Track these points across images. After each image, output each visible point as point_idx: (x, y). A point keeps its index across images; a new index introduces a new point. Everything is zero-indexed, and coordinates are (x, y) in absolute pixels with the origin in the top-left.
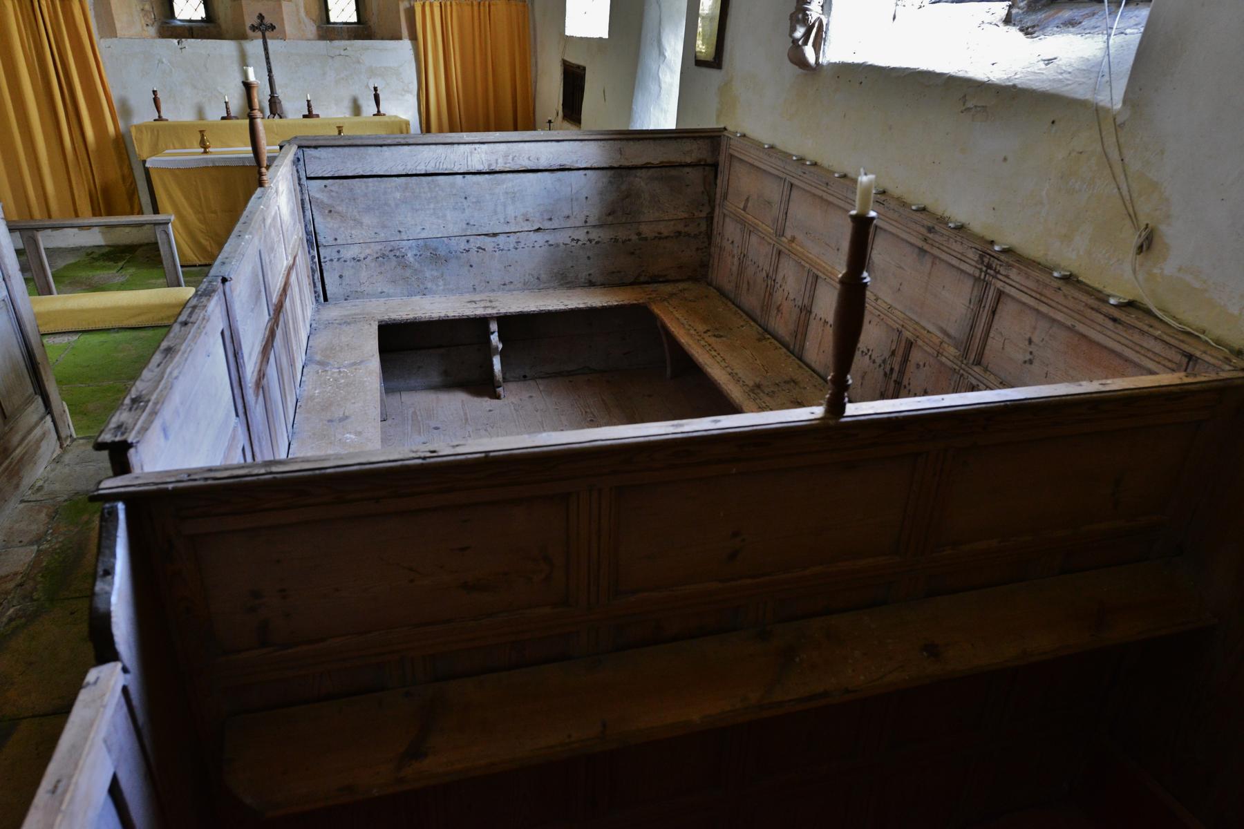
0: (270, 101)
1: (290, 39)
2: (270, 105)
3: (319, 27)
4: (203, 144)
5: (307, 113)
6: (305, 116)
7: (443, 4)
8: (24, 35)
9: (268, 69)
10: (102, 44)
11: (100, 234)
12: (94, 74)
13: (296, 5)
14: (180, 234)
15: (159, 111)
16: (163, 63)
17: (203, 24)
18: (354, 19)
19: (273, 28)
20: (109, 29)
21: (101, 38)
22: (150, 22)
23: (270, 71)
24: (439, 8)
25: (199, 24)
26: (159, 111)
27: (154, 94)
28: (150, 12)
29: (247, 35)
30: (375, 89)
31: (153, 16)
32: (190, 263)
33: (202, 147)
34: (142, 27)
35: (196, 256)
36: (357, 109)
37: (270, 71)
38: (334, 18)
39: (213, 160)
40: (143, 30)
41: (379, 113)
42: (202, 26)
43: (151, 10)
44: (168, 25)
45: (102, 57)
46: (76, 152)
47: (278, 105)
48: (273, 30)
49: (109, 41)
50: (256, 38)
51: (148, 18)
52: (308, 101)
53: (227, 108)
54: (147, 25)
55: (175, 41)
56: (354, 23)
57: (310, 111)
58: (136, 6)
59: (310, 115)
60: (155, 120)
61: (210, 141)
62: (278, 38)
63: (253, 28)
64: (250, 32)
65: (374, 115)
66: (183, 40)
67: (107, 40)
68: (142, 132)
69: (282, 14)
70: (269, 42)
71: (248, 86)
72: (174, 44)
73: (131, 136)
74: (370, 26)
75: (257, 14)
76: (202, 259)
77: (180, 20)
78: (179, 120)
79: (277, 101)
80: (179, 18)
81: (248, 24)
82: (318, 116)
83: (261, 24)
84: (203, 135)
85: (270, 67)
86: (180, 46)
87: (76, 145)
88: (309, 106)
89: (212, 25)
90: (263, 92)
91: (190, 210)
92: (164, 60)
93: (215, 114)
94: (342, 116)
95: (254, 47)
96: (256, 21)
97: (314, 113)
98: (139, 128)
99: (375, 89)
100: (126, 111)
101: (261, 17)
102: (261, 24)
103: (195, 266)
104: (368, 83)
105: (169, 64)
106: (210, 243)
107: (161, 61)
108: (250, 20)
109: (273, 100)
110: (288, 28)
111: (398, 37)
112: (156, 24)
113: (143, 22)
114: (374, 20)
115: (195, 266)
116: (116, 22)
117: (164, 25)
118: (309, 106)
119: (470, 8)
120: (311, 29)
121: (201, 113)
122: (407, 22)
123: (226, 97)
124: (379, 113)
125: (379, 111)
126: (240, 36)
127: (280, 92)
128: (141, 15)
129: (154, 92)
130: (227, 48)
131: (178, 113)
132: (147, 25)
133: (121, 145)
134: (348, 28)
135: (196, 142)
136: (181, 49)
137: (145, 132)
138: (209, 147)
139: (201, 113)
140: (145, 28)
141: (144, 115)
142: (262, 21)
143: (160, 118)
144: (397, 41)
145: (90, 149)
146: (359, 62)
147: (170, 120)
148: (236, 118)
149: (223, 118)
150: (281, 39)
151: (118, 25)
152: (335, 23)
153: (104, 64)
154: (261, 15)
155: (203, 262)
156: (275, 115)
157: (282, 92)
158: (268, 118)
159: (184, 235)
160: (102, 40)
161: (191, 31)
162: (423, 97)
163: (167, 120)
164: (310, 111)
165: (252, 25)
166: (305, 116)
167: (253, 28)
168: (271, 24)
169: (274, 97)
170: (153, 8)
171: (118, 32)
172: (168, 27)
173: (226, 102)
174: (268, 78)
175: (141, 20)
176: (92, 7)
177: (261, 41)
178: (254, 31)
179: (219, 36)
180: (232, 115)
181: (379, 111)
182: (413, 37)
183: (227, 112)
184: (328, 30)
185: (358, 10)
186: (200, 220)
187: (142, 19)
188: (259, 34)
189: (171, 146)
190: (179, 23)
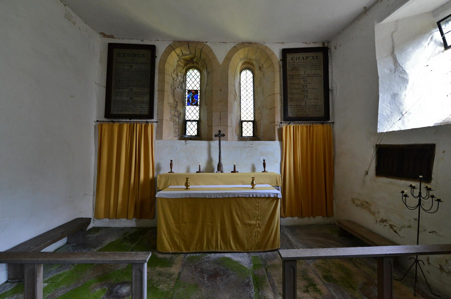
0: (218, 165)
1: (229, 141)
2: (218, 167)
3: (238, 138)
4: (187, 185)
5: (233, 171)
6: (232, 172)
7: (295, 126)
8: (128, 138)
9: (219, 152)
10: (155, 142)
11: (135, 221)
12: (150, 152)
13: (233, 129)
14: (165, 235)
15: (171, 169)
16: (177, 149)
17: (196, 137)
18: (252, 135)
19: (224, 135)
20: (160, 136)
21: (156, 140)
22: (176, 136)
23: (220, 153)
24: (293, 128)
25: (194, 137)
26: (171, 169)
27: (171, 162)
28: (177, 132)
29: (212, 139)
30: (264, 160)
31: (178, 134)
32: (167, 252)
33: (186, 186)
34: (173, 137)
35: (171, 248)
36: (254, 169)
37: (220, 153)
38: (244, 135)
39: (190, 194)
40: (173, 138)
41: (265, 171)
42: (195, 138)
43: (178, 131)
44: (182, 137)
45: (154, 147)
46: (135, 187)
47: (221, 167)
48: (224, 136)
49: (159, 141)
50: (216, 140)
51: (176, 134)
52: (234, 165)
53: (200, 168)
54: (175, 136)
55: (184, 141)
56: (252, 137)
57: (234, 169)
58: (173, 129)
59: (234, 171)
60: (169, 172)
61: (190, 183)
62: (224, 140)
63: (216, 136)
64: (214, 137)
65: (262, 172)
66: (187, 141)
67: (158, 140)
68: (162, 178)
69: (228, 131)
70: (221, 141)
71: (297, 79)
72: (183, 142)
73: (157, 179)
74: (259, 138)
75: (218, 130)
76: (173, 250)
77: (188, 136)
78: (179, 173)
79: (221, 165)
80: (187, 135)
81: (214, 134)
82: (238, 172)
83: (220, 134)
84: (253, 179)
85: (220, 151)
86: (186, 143)
87: (135, 182)
88: (234, 167)
89: (199, 137)
90: (215, 161)
91: (173, 222)
92: (178, 148)
93: (194, 170)
94: (247, 172)
95: (215, 144)
96: (217, 133)
97: (236, 170)
98: (161, 176)
99: (264, 160)
100: (159, 169)
101: (220, 131)
102: (220, 134)
103: (169, 253)
104: (259, 158)
105: (180, 150)
106: (179, 241)
107: (177, 149)
108: (215, 132)
109: (220, 165)
110: (229, 136)
111: (273, 139)
112: (178, 136)
113: (174, 135)
114: (261, 135)
115: (169, 253)
116: (163, 134)
117: (182, 137)
118: (234, 167)
119: (306, 128)
120: (236, 137)
121: (188, 170)
122: (278, 134)
123: (200, 163)
124: (265, 171)
125: (265, 170)
126: (210, 139)
127: (222, 161)
128: (174, 133)
129: (171, 161)
130: (204, 144)
131: (179, 170)
132: (175, 136)
133: (154, 181)
134: (250, 138)
135: (184, 183)
136: (186, 144)
137: (163, 177)
138: (189, 186)
139: (188, 170)
140: (174, 137)
141: (165, 170)
142: (220, 133)
143: (171, 172)
144: (273, 141)
145: (140, 184)
146: (257, 150)
147: (268, 172)
148: (203, 172)
149: (197, 172)
150: (226, 140)
151: (164, 135)
152: (244, 137)
153: (155, 149)
154: (220, 130)
155: (174, 251)
156: (219, 171)
157: (223, 162)
158: (216, 172)
159: (167, 236)
160: (156, 141)
161: (191, 138)
162: (283, 164)
163: (174, 172)
164: (234, 169)
165: (216, 134)
166: (232, 172)
167: (216, 136)
168: (224, 134)
169: (220, 163)
170: (179, 131)
171: (163, 138)
172: (183, 138)
173: (199, 165)
174: (219, 155)
175: (173, 135)
176: (156, 129)
177: (218, 141)
178: (216, 137)
179: (201, 139)
180: (201, 171)
181: (265, 170)
182: (281, 139)
183: (199, 170)
184: (241, 138)
185: (253, 132)
186: (176, 227)
187: (174, 134)
188: (218, 138)
189: (175, 183)
190: (187, 136)
